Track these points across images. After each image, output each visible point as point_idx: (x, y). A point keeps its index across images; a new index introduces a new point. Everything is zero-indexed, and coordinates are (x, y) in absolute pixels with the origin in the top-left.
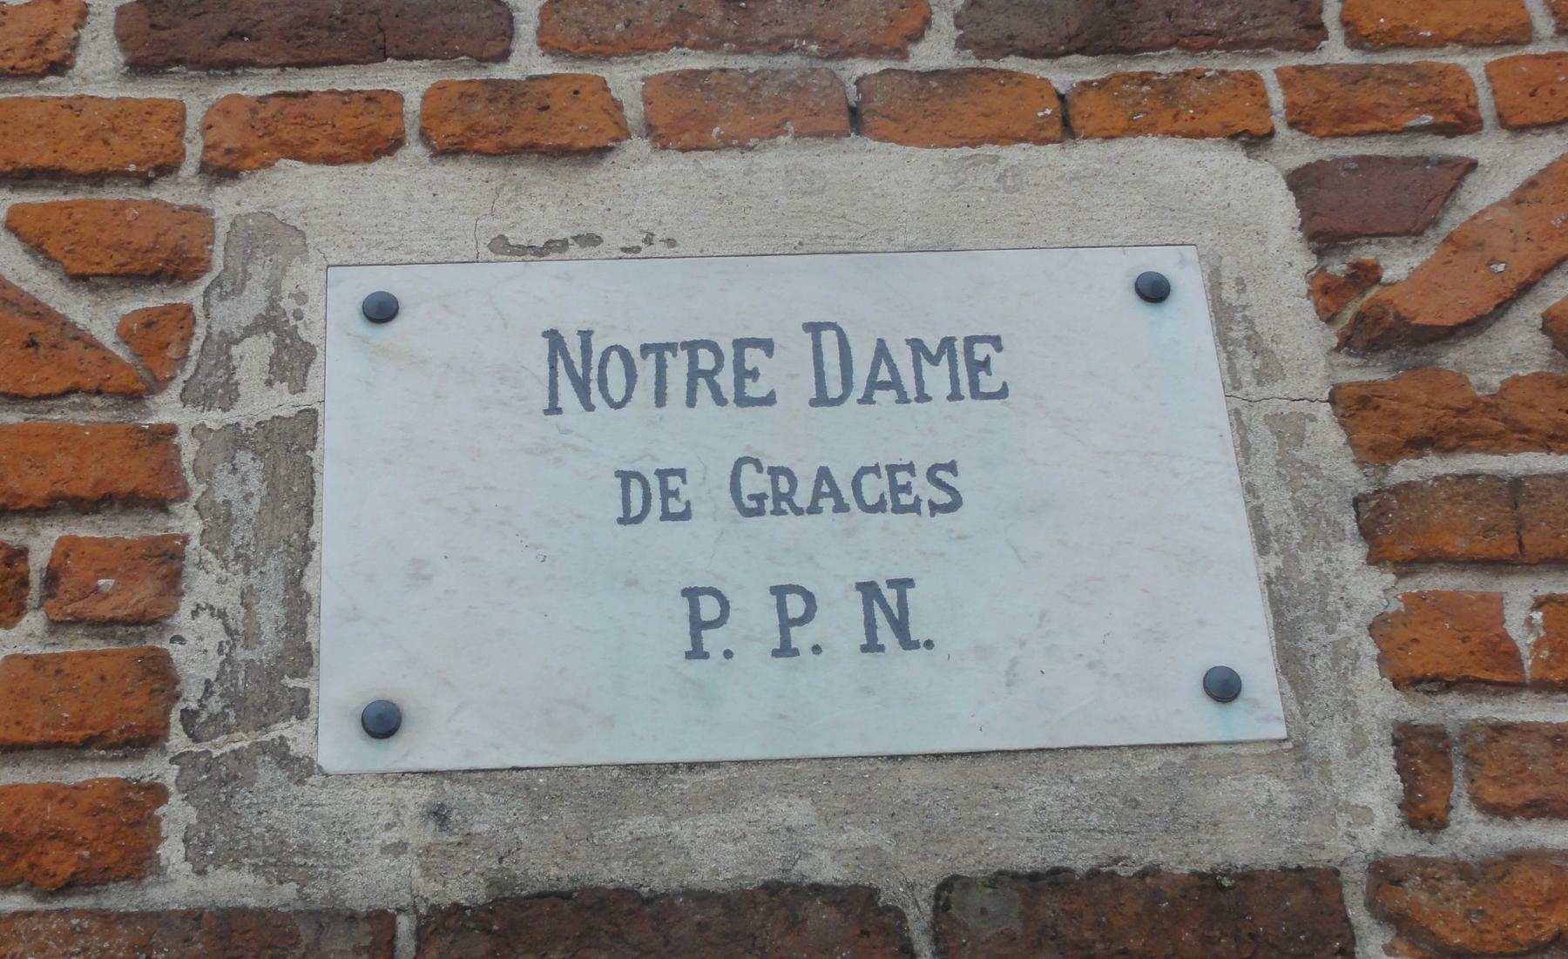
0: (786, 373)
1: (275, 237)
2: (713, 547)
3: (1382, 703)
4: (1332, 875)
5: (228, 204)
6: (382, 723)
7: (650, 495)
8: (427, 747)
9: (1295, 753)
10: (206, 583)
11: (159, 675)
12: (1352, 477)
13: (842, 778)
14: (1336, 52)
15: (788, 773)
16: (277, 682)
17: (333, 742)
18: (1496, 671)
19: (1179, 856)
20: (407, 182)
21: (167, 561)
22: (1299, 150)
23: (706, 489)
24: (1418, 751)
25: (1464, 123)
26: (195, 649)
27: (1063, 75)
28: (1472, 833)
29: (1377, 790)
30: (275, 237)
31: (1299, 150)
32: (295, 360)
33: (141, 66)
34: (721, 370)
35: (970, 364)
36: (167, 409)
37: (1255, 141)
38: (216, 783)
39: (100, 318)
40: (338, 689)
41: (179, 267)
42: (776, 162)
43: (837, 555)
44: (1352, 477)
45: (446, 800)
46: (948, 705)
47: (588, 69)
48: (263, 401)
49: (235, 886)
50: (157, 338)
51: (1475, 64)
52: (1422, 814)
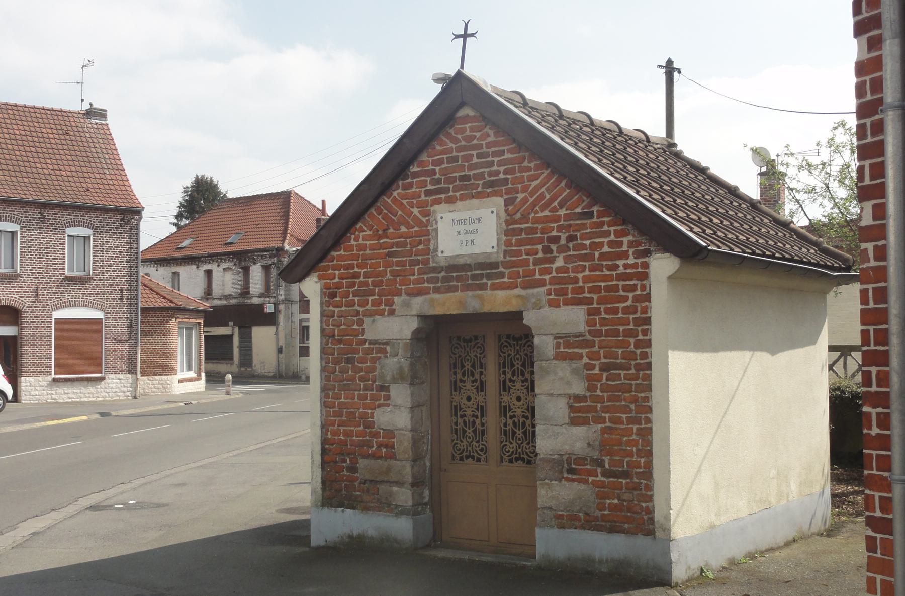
0: (467, 222)
1: (435, 211)
2: (463, 238)
3: (504, 248)
4: (881, 49)
5: (432, 209)
6: (442, 252)
7: (459, 233)
8: (445, 254)
9: (497, 253)
10: (432, 242)
11: (429, 249)
12: (505, 228)
13: (470, 256)
14: (510, 186)
15: (466, 255)
16: (436, 250)
17: (440, 254)
18: (511, 245)
19: (489, 261)
20: (443, 206)
21: (429, 241)
22: (505, 197)
23: (462, 232)
24: (505, 252)
25: (517, 193)
26: (432, 247)
27: (489, 190)
28: (508, 258)
29: (502, 256)
30: (435, 211)
31: (505, 197)
32: (437, 223)
33: (426, 196)
34: (462, 222)
35: (479, 220)
36: (429, 228)
37: (502, 196)
38: (433, 257)
39: (424, 220)
40: (440, 250)
41: (429, 215)
42: (468, 202)
43: (470, 237)
44: (505, 228)
45: (446, 258)
46: (476, 250)
47: (613, 426)
48: (435, 227)
49: (434, 265)
50: (428, 221)
51: (520, 186)
52: (505, 257)
